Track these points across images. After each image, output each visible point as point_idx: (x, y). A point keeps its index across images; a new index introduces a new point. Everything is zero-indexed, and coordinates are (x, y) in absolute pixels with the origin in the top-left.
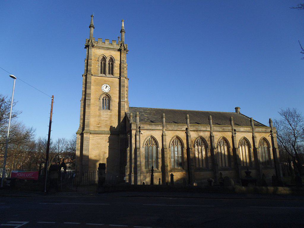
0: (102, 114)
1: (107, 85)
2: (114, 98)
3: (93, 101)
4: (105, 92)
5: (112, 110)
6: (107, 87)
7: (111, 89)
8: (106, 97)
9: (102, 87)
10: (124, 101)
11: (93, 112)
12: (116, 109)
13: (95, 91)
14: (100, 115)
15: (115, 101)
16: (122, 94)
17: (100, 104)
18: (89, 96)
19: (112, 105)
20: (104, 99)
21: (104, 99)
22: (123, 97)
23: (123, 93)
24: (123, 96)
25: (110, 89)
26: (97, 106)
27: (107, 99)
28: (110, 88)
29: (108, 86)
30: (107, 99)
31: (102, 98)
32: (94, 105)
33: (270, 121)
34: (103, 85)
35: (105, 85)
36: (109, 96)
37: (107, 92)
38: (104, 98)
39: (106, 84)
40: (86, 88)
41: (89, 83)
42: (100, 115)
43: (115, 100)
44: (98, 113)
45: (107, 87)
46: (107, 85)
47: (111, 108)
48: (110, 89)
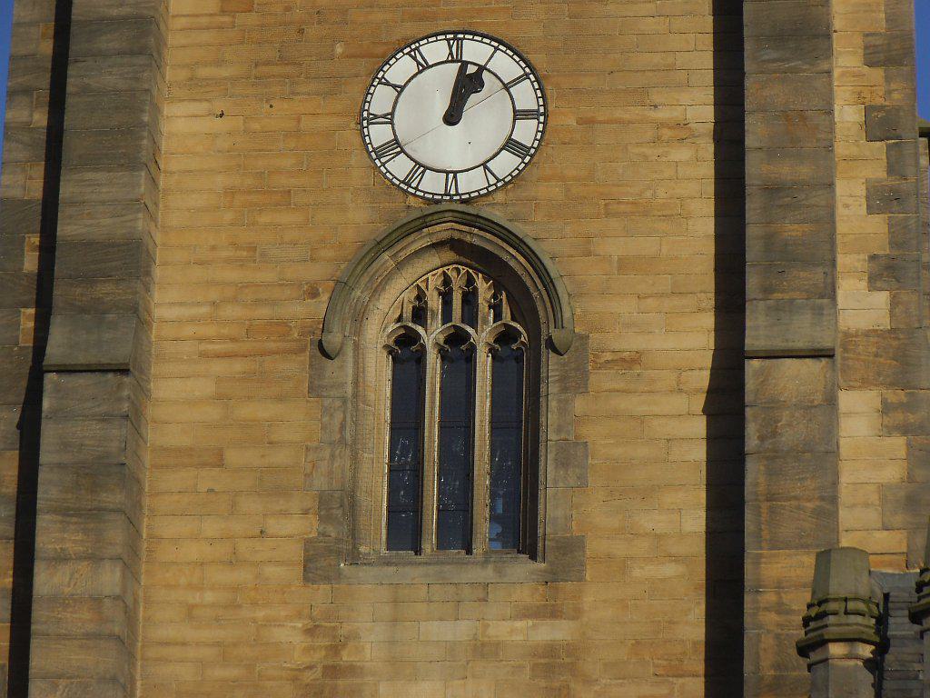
0: (370, 645)
1: (475, 51)
2: (624, 308)
3: (204, 387)
4: (432, 184)
5: (572, 547)
6: (468, 83)
7: (565, 119)
8: (470, 298)
9: (381, 100)
10: (803, 332)
11: (190, 612)
12: (652, 521)
13: (231, 192)
14: (333, 671)
15: (632, 361)
16: (773, 190)
17: (352, 446)
18: (105, 290)
19: (574, 453)
20: (432, 335)
21: (432, 335)
22: (785, 257)
23: (785, 171)
24: (792, 230)
25: (526, 132)
26: (272, 486)
27: (482, 337)
28: (526, 96)
29: (505, 65)
30: (482, 337)
31: (378, 332)
32: (208, 479)
33: (886, 596)
34: (401, 68)
35: (435, 50)
36: (515, 261)
37: (471, 183)
38: (420, 314)
39: (456, 35)
40: (177, 644)
41: (108, 42)
42: (333, 671)
43: (631, 343)
44: (290, 635)
45: (468, 83)
46: (475, 51)
47: (554, 509)
48: (526, 132)
